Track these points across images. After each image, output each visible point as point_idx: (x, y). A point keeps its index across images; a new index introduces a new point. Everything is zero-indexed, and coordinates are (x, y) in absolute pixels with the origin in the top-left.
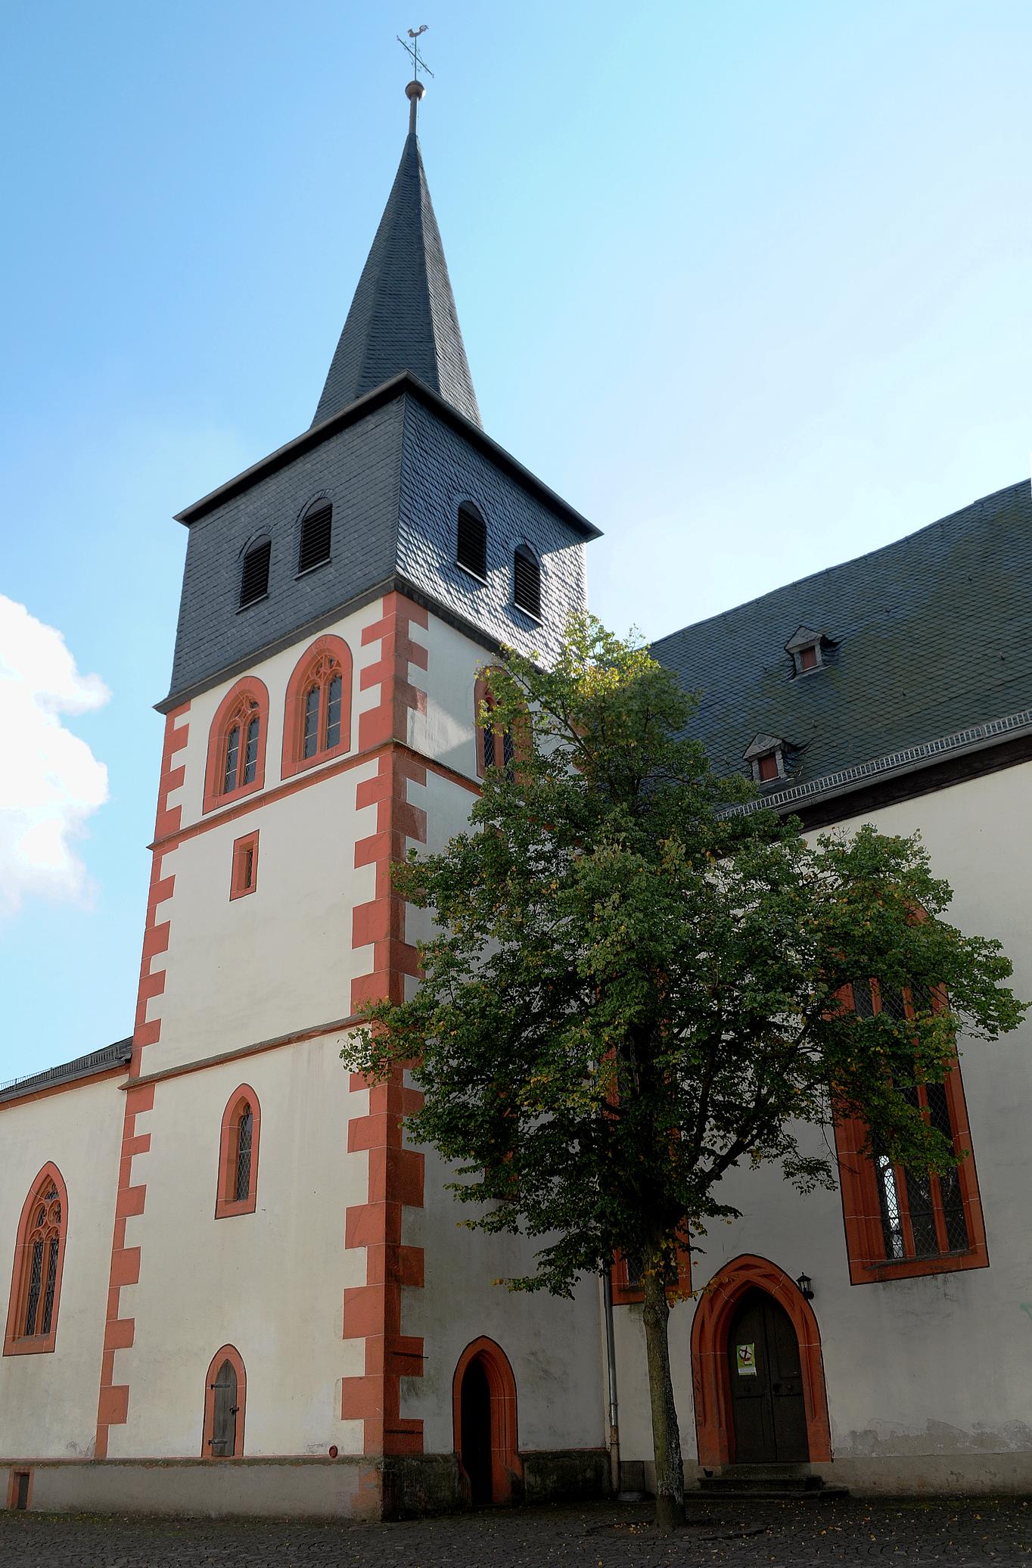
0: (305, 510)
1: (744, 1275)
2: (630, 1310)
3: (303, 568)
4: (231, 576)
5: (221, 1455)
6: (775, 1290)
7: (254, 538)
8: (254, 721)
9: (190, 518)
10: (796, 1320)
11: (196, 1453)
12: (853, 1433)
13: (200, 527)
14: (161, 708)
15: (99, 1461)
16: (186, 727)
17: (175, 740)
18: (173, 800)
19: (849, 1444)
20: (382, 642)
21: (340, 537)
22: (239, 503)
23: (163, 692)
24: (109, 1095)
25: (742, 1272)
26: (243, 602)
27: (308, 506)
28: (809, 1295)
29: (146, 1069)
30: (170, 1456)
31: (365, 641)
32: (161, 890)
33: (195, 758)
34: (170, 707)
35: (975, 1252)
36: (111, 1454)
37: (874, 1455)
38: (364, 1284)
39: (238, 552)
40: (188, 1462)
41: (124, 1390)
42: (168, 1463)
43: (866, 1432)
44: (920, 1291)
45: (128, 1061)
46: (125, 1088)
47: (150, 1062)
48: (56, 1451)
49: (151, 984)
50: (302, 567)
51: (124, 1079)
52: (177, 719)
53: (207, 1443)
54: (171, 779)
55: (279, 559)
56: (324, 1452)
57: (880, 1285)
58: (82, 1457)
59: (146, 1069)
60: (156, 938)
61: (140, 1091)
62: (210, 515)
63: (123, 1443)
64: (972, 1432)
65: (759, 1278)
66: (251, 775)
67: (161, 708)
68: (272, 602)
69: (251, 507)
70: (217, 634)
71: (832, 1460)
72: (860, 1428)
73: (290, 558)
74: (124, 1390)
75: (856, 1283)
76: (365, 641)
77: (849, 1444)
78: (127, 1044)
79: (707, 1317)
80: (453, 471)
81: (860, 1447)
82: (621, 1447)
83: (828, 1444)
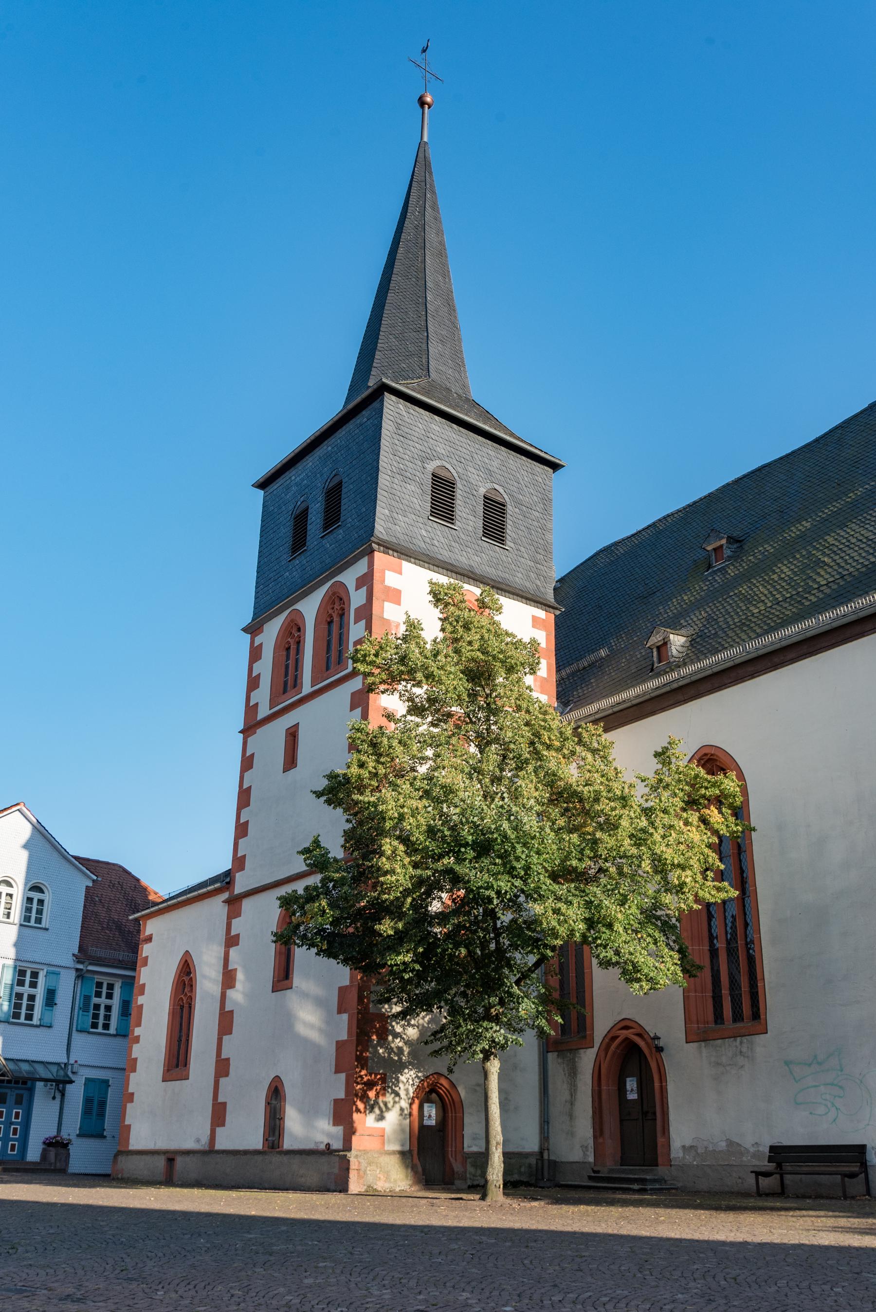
0: (327, 484)
1: (625, 1033)
2: (558, 1055)
3: (294, 552)
4: (286, 531)
5: (273, 1148)
6: (642, 1044)
7: (299, 503)
8: (298, 643)
9: (263, 485)
10: (653, 1065)
11: (259, 1145)
12: (684, 1147)
13: (280, 483)
14: (245, 630)
15: (210, 1152)
16: (261, 645)
17: (255, 654)
18: (255, 697)
19: (681, 1155)
20: (367, 590)
21: (346, 506)
22: (291, 474)
23: (247, 617)
24: (217, 906)
25: (624, 1032)
26: (293, 552)
27: (329, 480)
28: (660, 1049)
29: (238, 889)
30: (247, 1148)
31: (357, 588)
32: (247, 763)
33: (265, 668)
34: (253, 629)
35: (585, 1037)
36: (218, 1147)
37: (695, 1163)
38: (346, 1038)
39: (290, 513)
40: (256, 1152)
41: (224, 1104)
42: (246, 1152)
43: (691, 1147)
44: (727, 1048)
45: (228, 883)
46: (227, 902)
47: (241, 884)
48: (189, 1144)
49: (242, 830)
50: (326, 527)
51: (225, 896)
52: (256, 638)
53: (266, 1140)
54: (253, 683)
55: (312, 520)
56: (322, 1147)
57: (703, 1044)
58: (202, 1148)
59: (238, 889)
60: (244, 797)
61: (234, 904)
62: (274, 483)
63: (225, 1140)
64: (752, 1150)
65: (633, 1036)
66: (297, 683)
67: (245, 630)
68: (309, 553)
69: (298, 478)
70: (279, 575)
71: (671, 1165)
72: (688, 1143)
73: (318, 520)
74: (224, 1104)
75: (156, 1157)
76: (357, 588)
77: (681, 1155)
78: (228, 873)
79: (602, 1062)
80: (426, 446)
81: (687, 1157)
82: (550, 1152)
83: (669, 1154)
